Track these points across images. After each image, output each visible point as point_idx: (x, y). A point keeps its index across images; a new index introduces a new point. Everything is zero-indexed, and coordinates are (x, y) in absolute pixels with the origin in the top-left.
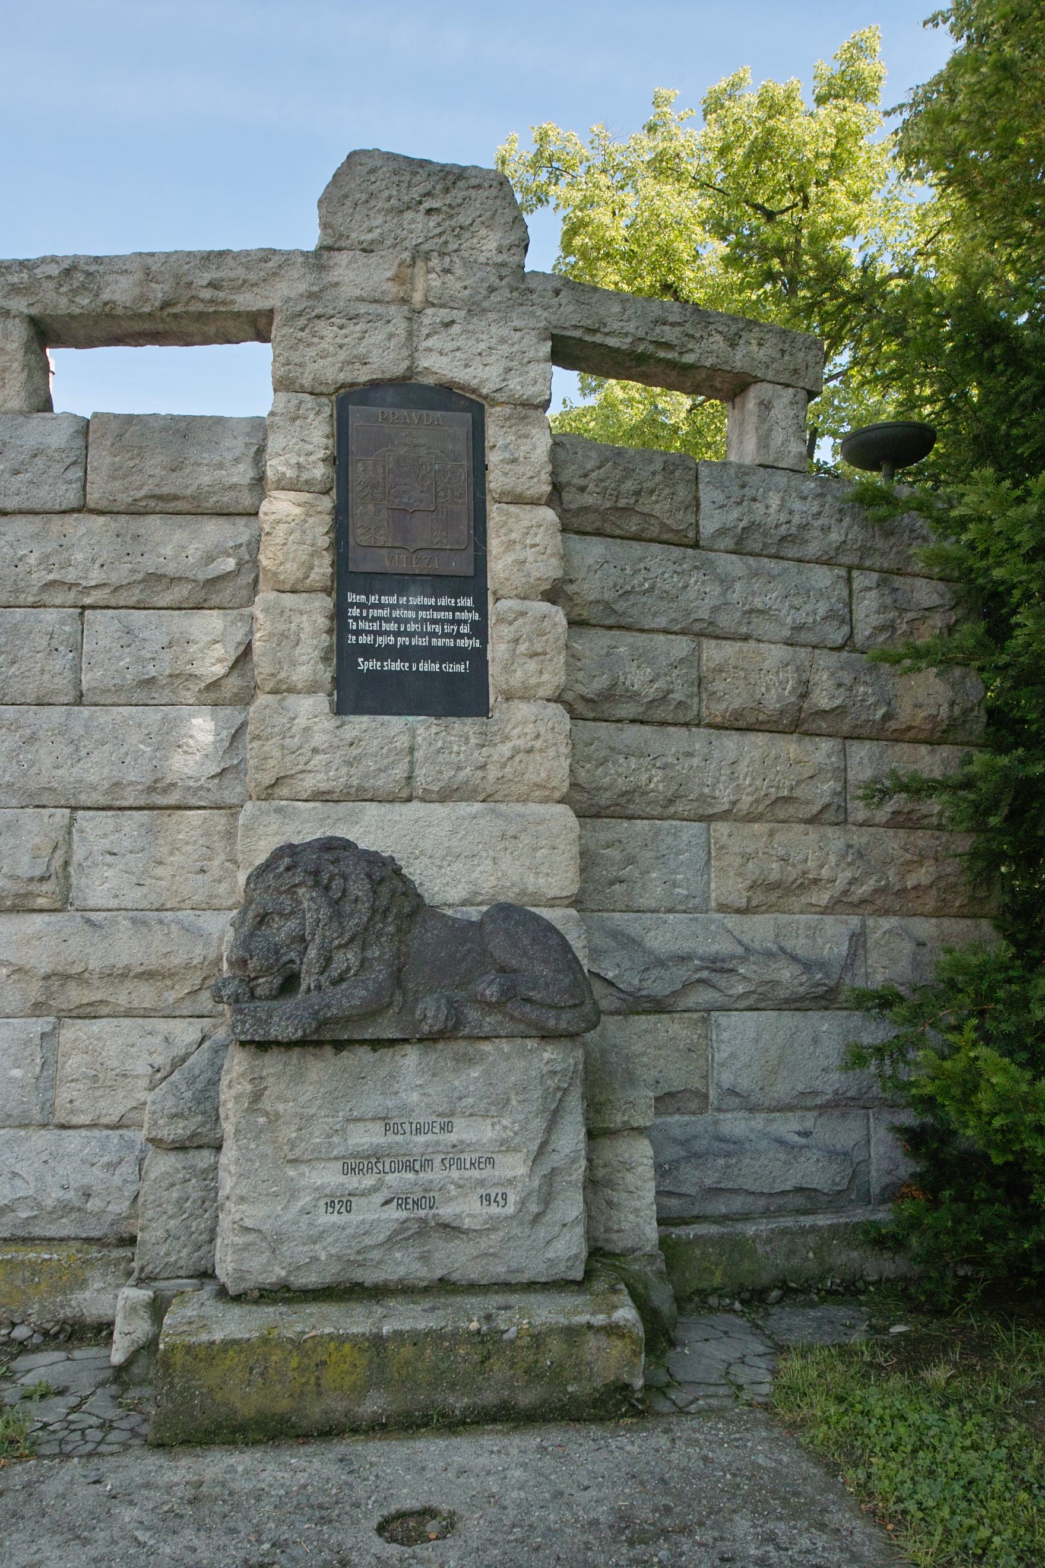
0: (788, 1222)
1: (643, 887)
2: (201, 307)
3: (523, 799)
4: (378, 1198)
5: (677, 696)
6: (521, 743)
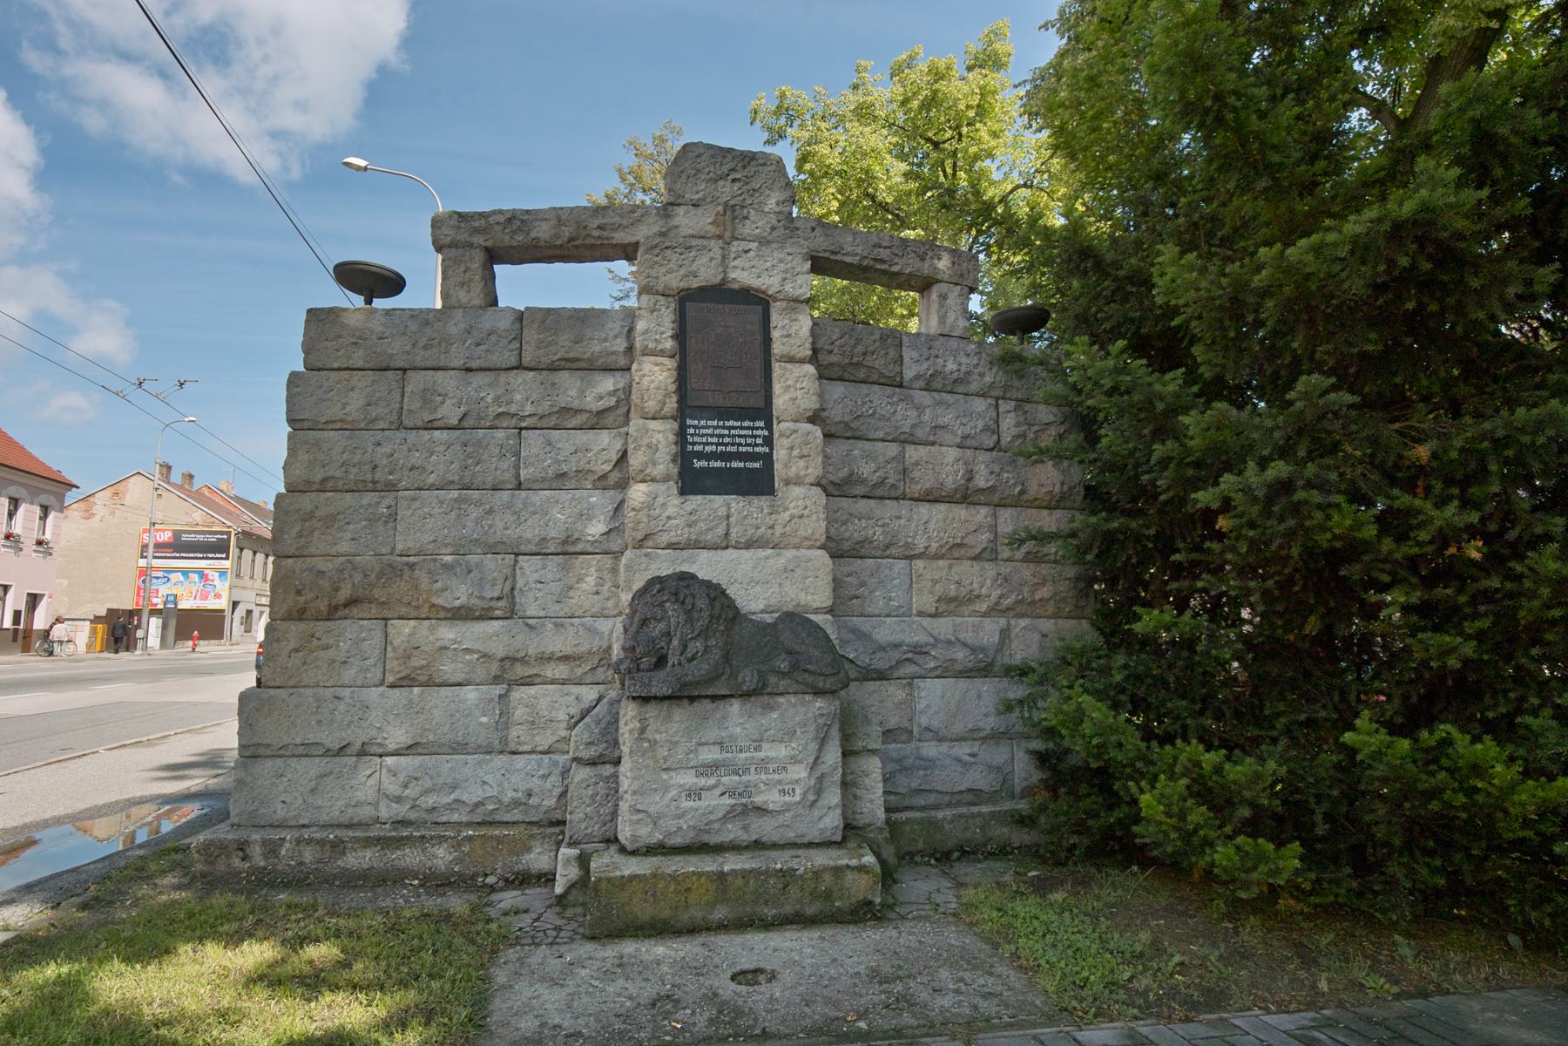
0: (963, 810)
2: (592, 241)
3: (797, 547)
4: (718, 792)
5: (891, 481)
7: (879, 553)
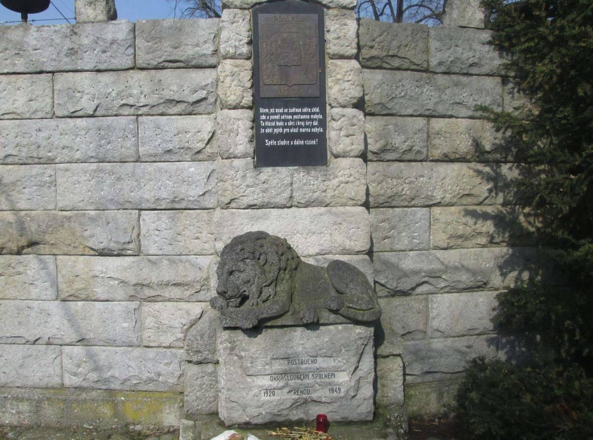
1: (399, 240)
4: (286, 390)
5: (416, 148)
6: (342, 179)
7: (406, 204)
